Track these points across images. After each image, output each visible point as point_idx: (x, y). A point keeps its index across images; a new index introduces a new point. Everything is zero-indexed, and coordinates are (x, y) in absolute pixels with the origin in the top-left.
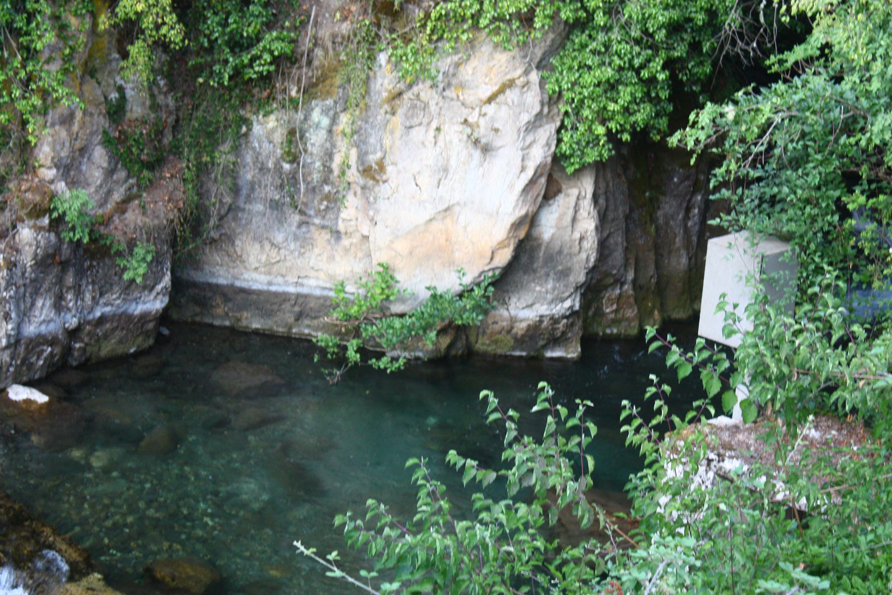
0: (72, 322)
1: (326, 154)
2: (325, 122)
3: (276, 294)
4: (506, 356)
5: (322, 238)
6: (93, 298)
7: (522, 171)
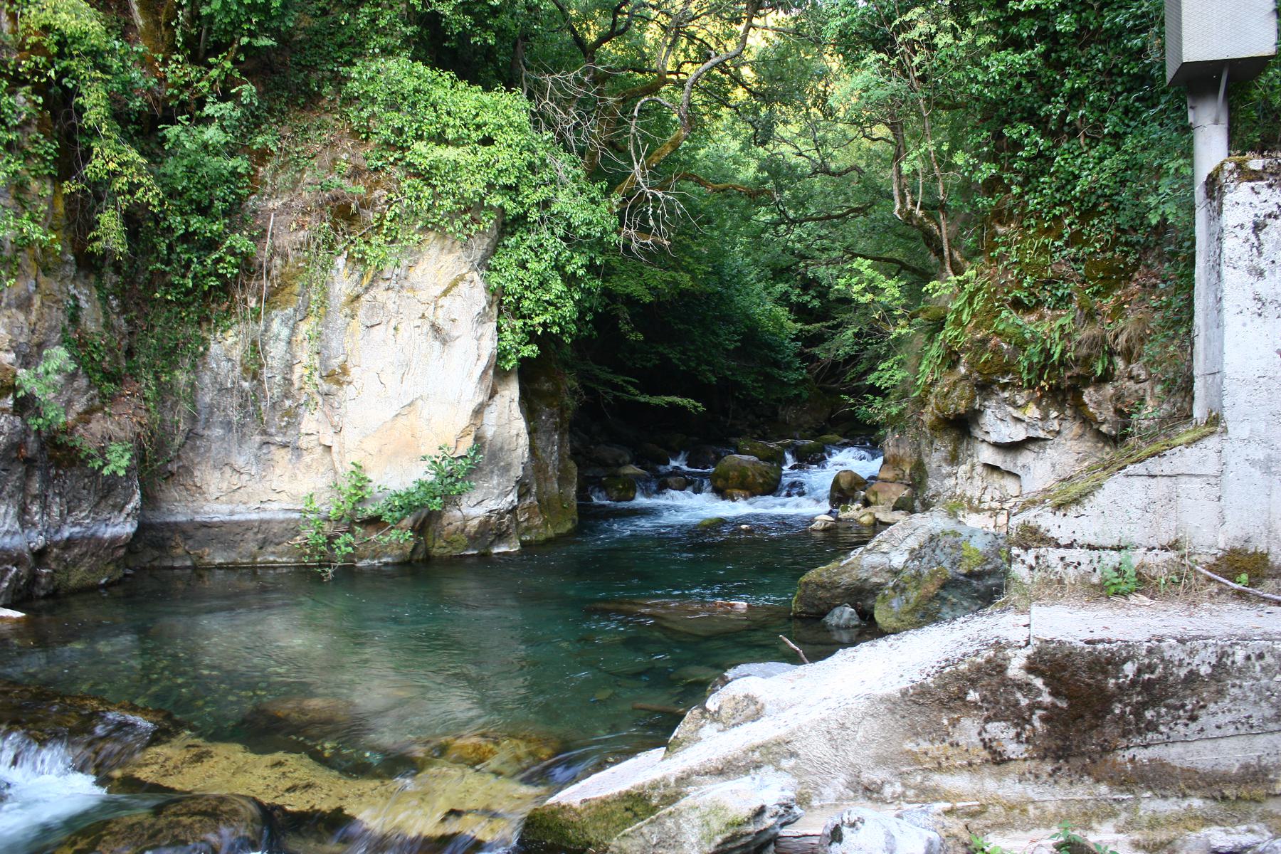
0: (39, 541)
2: (285, 333)
3: (238, 524)
4: (461, 556)
5: (282, 456)
6: (61, 514)
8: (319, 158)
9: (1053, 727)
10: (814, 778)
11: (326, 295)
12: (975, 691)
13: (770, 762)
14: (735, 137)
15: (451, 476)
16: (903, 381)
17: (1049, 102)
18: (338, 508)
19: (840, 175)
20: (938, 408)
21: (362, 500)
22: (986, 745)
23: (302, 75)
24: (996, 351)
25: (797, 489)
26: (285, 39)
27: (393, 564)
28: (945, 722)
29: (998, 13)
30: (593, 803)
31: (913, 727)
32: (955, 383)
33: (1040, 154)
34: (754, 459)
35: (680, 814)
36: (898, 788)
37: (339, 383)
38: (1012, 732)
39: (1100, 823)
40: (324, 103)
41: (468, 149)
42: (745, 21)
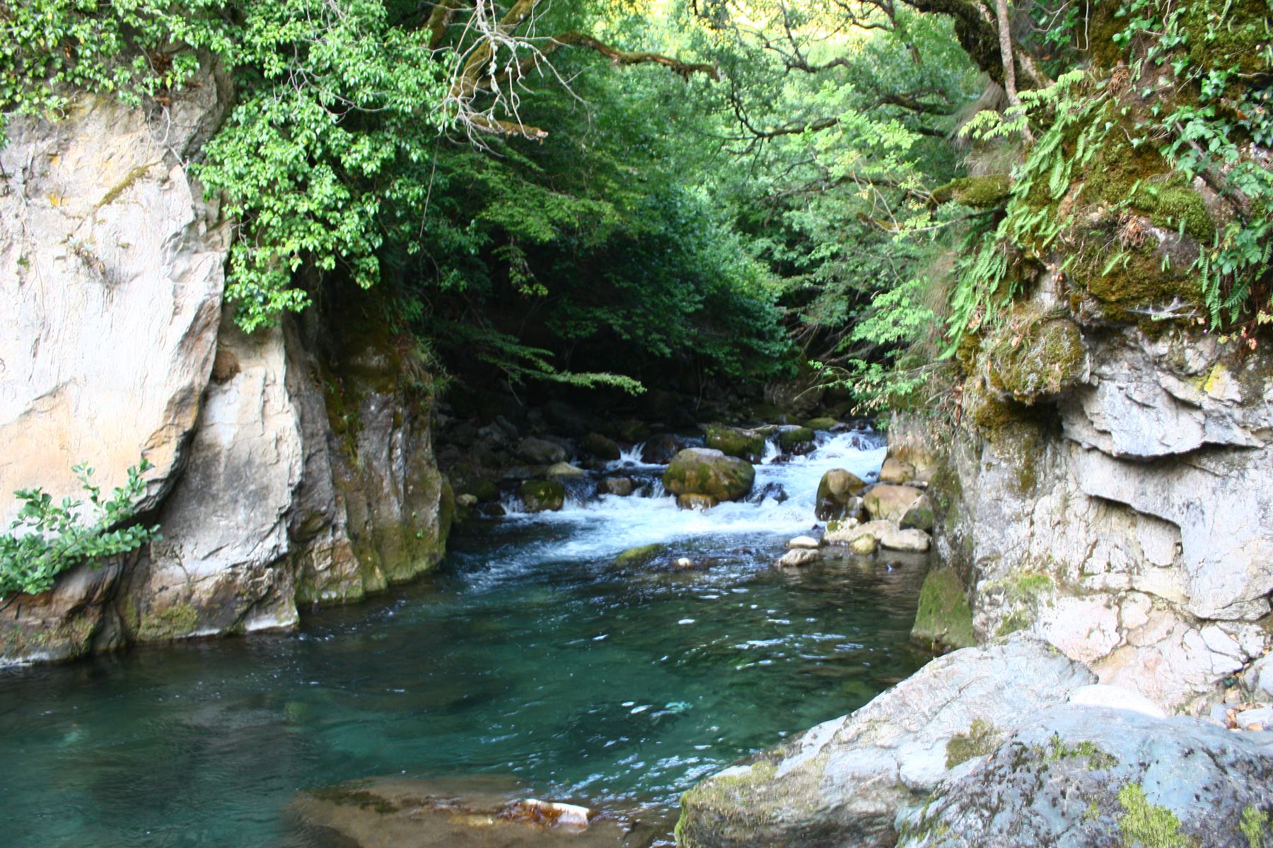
4: (189, 639)
7: (175, 314)
20: (998, 382)
34: (717, 453)
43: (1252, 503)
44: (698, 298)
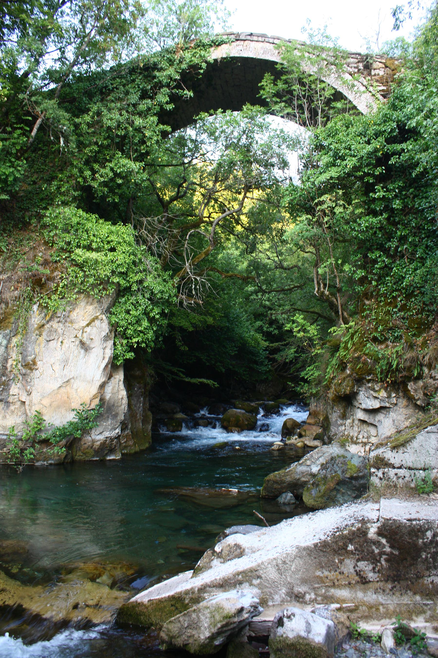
1: (4, 360)
4: (90, 461)
8: (27, 254)
9: (391, 564)
10: (270, 590)
11: (27, 324)
12: (352, 545)
13: (247, 581)
14: (237, 249)
15: (87, 419)
16: (319, 375)
17: (390, 241)
18: (27, 434)
19: (289, 269)
20: (336, 391)
21: (40, 430)
22: (358, 573)
23: (21, 213)
24: (365, 363)
25: (265, 428)
26: (14, 196)
27: (55, 465)
28: (337, 561)
29: (365, 198)
30: (155, 601)
31: (320, 563)
32: (344, 378)
33: (386, 266)
34: (243, 411)
35: (199, 611)
36: (313, 596)
37: (31, 369)
38: (371, 567)
39: (417, 616)
40: (31, 227)
41: (103, 253)
42: (243, 194)
43: (391, 420)
44: (235, 349)
